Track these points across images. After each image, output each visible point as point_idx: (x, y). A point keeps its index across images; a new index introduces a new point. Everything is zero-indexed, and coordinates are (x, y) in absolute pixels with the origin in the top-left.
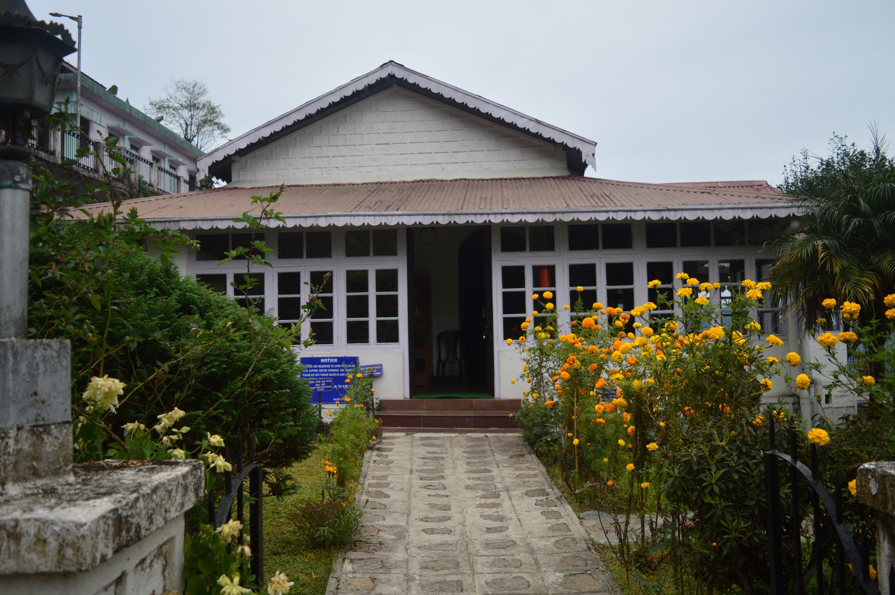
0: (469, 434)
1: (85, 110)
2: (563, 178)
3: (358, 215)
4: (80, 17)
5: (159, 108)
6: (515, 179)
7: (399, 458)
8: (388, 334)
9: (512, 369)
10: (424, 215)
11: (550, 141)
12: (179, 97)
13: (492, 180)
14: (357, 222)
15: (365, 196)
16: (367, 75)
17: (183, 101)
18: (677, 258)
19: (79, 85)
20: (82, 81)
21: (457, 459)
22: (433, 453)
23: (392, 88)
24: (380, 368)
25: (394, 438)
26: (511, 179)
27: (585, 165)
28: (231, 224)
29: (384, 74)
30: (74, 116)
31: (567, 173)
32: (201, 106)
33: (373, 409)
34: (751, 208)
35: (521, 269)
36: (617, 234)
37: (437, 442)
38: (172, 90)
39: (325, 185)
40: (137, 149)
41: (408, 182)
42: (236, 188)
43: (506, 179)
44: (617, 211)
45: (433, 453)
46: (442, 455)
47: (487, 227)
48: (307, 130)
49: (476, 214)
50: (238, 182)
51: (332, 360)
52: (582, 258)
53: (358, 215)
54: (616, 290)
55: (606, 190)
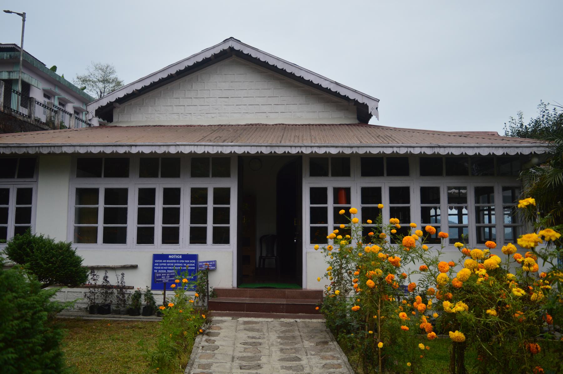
0: (282, 320)
1: (27, 77)
2: (354, 125)
3: (200, 145)
4: (24, 13)
5: (83, 81)
6: (319, 125)
7: (223, 343)
8: (221, 237)
9: (317, 266)
10: (251, 146)
11: (346, 98)
12: (97, 74)
13: (303, 125)
14: (200, 150)
15: (209, 133)
16: (214, 47)
17: (99, 77)
18: (444, 185)
19: (21, 59)
20: (23, 56)
21: (272, 345)
22: (253, 338)
23: (231, 57)
24: (214, 264)
25: (222, 321)
26: (316, 125)
27: (370, 116)
28: (101, 149)
29: (226, 47)
30: (17, 80)
31: (357, 122)
32: (111, 81)
33: (208, 295)
34: (502, 147)
35: (325, 190)
36: (397, 165)
37: (257, 326)
38: (92, 70)
39: (181, 126)
40: (63, 106)
41: (242, 125)
42: (116, 126)
43: (313, 125)
44: (400, 147)
45: (253, 338)
46: (260, 341)
47: (299, 157)
48: (169, 86)
49: (291, 147)
50: (117, 122)
51: (177, 257)
52: (371, 182)
53: (200, 145)
54: (89, 208)
55: (388, 133)
